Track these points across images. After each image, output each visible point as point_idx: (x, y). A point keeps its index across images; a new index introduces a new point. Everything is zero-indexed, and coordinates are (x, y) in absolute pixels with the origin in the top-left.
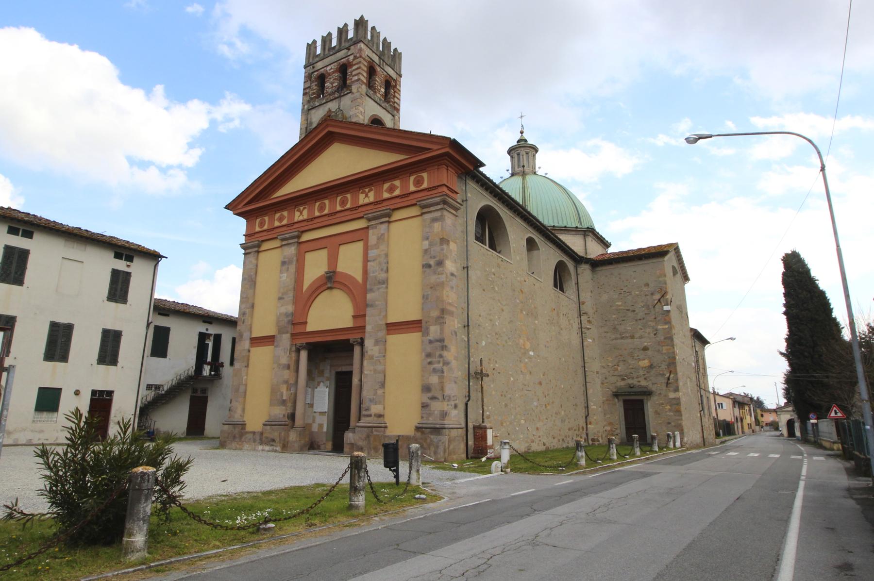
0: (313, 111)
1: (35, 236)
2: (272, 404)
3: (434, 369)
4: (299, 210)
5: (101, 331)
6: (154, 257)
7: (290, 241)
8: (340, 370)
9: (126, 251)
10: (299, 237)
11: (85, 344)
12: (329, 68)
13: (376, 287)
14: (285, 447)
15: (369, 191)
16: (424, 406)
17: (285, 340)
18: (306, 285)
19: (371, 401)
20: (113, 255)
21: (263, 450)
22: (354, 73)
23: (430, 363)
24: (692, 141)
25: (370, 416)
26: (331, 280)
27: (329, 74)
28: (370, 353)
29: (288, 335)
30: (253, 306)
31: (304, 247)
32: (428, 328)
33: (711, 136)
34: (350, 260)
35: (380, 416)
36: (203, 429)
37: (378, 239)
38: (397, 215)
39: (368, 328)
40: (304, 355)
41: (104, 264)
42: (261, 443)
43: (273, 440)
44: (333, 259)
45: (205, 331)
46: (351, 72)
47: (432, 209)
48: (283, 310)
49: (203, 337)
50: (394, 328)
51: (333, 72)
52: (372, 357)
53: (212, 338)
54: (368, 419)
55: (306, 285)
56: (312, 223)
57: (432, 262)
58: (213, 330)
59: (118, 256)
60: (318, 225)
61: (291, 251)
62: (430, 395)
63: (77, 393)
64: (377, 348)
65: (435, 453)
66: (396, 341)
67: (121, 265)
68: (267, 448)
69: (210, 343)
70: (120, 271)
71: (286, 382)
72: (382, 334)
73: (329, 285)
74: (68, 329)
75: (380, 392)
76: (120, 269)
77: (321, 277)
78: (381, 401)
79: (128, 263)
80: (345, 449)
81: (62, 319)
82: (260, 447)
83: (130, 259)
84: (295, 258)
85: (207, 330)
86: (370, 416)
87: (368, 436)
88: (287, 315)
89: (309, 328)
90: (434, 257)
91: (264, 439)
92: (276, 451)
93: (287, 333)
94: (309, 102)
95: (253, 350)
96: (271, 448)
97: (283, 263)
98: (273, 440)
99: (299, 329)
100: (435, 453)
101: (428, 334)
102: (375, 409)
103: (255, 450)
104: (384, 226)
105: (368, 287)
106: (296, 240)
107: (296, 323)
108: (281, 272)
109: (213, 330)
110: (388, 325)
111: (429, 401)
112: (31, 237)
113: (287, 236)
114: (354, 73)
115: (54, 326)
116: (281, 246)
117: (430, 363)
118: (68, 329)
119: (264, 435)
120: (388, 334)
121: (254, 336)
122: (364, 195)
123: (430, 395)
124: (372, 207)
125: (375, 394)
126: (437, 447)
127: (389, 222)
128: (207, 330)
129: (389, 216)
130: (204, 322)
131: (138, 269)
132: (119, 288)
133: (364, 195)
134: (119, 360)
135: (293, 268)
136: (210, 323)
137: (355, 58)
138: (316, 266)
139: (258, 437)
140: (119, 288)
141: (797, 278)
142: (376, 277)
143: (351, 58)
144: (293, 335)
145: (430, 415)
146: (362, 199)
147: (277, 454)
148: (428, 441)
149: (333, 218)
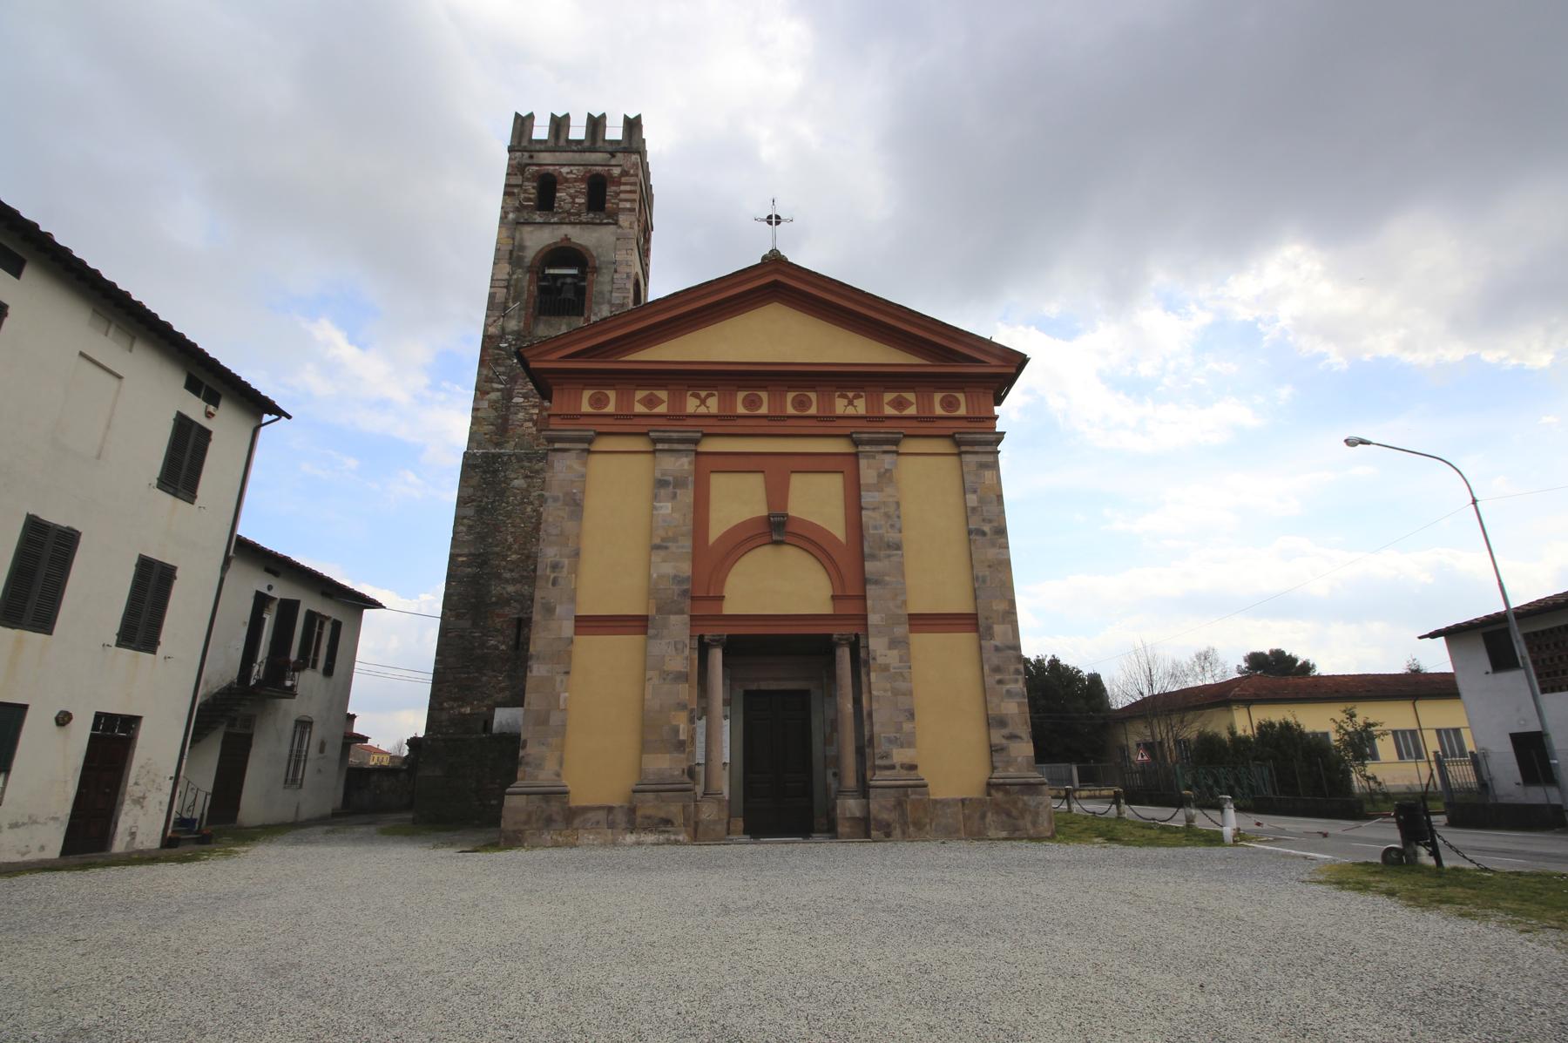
0: (528, 229)
1: (27, 272)
2: (645, 747)
3: (1008, 691)
4: (697, 396)
5: (135, 560)
6: (257, 406)
7: (676, 446)
8: (754, 687)
9: (209, 378)
10: (696, 442)
11: (96, 591)
12: (565, 170)
13: (882, 553)
14: (698, 834)
15: (708, 396)
16: (994, 750)
17: (679, 626)
18: (716, 531)
19: (890, 741)
20: (183, 381)
21: (639, 844)
22: (622, 196)
23: (1000, 682)
24: (1350, 443)
25: (893, 767)
26: (777, 528)
27: (567, 180)
28: (880, 660)
29: (686, 618)
30: (577, 554)
31: (708, 465)
32: (989, 628)
33: (1369, 443)
34: (817, 501)
35: (913, 767)
36: (236, 808)
37: (880, 476)
38: (909, 446)
39: (873, 619)
40: (717, 656)
41: (162, 397)
42: (632, 828)
43: (667, 822)
44: (777, 492)
45: (265, 591)
46: (618, 194)
47: (976, 448)
48: (668, 569)
49: (261, 601)
50: (589, 624)
51: (576, 180)
52: (885, 668)
53: (274, 607)
54: (888, 773)
55: (716, 531)
56: (726, 424)
57: (986, 528)
58: (281, 590)
59: (193, 386)
60: (759, 431)
61: (680, 464)
62: (1005, 732)
63: (63, 719)
64: (895, 653)
65: (1034, 824)
66: (925, 643)
67: (195, 408)
68: (651, 838)
69: (269, 619)
70: (192, 422)
71: (682, 706)
72: (901, 630)
73: (775, 537)
74: (67, 541)
75: (907, 727)
76: (193, 417)
77: (752, 521)
78: (909, 742)
79: (211, 408)
80: (840, 829)
81: (56, 516)
82: (630, 838)
83: (212, 399)
84: (691, 479)
85: (270, 588)
86: (893, 767)
87: (900, 804)
88: (677, 579)
89: (729, 608)
90: (990, 521)
91: (639, 820)
92: (676, 842)
93: (681, 612)
94: (518, 210)
95: (578, 639)
96: (662, 838)
97: (661, 483)
98: (667, 822)
99: (705, 609)
100: (1034, 824)
101: (992, 637)
102: (900, 756)
103: (614, 844)
104: (888, 458)
105: (866, 550)
106: (692, 447)
107: (701, 595)
108: (655, 497)
109: (281, 590)
110: (912, 617)
111: (1004, 741)
112: (17, 273)
113: (675, 435)
114: (622, 196)
115: (35, 529)
116: (654, 452)
117: (1000, 682)
118: (67, 541)
119: (639, 813)
120: (911, 631)
121: (582, 612)
122: (845, 402)
123: (1005, 732)
124: (864, 423)
125: (899, 729)
126: (1037, 814)
127: (589, 452)
128: (270, 588)
129: (590, 441)
130: (268, 570)
131: (224, 424)
132: (183, 465)
133: (845, 402)
134: (162, 639)
135: (687, 496)
136: (276, 574)
137: (625, 173)
138: (737, 501)
139: (620, 818)
140: (183, 465)
141: (379, 606)
142: (881, 537)
143: (616, 171)
144: (693, 618)
145: (1008, 763)
146: (841, 407)
147: (682, 850)
148: (1020, 805)
149: (776, 426)
